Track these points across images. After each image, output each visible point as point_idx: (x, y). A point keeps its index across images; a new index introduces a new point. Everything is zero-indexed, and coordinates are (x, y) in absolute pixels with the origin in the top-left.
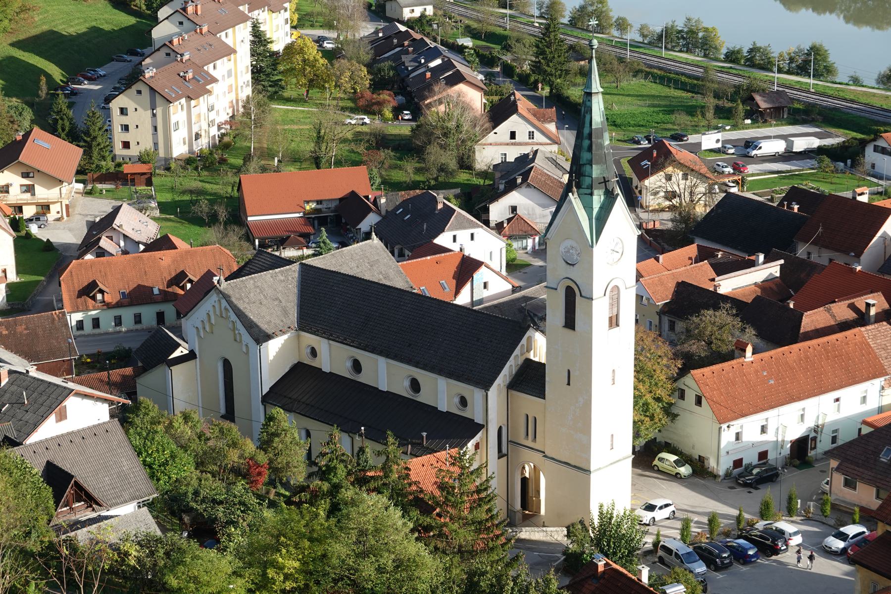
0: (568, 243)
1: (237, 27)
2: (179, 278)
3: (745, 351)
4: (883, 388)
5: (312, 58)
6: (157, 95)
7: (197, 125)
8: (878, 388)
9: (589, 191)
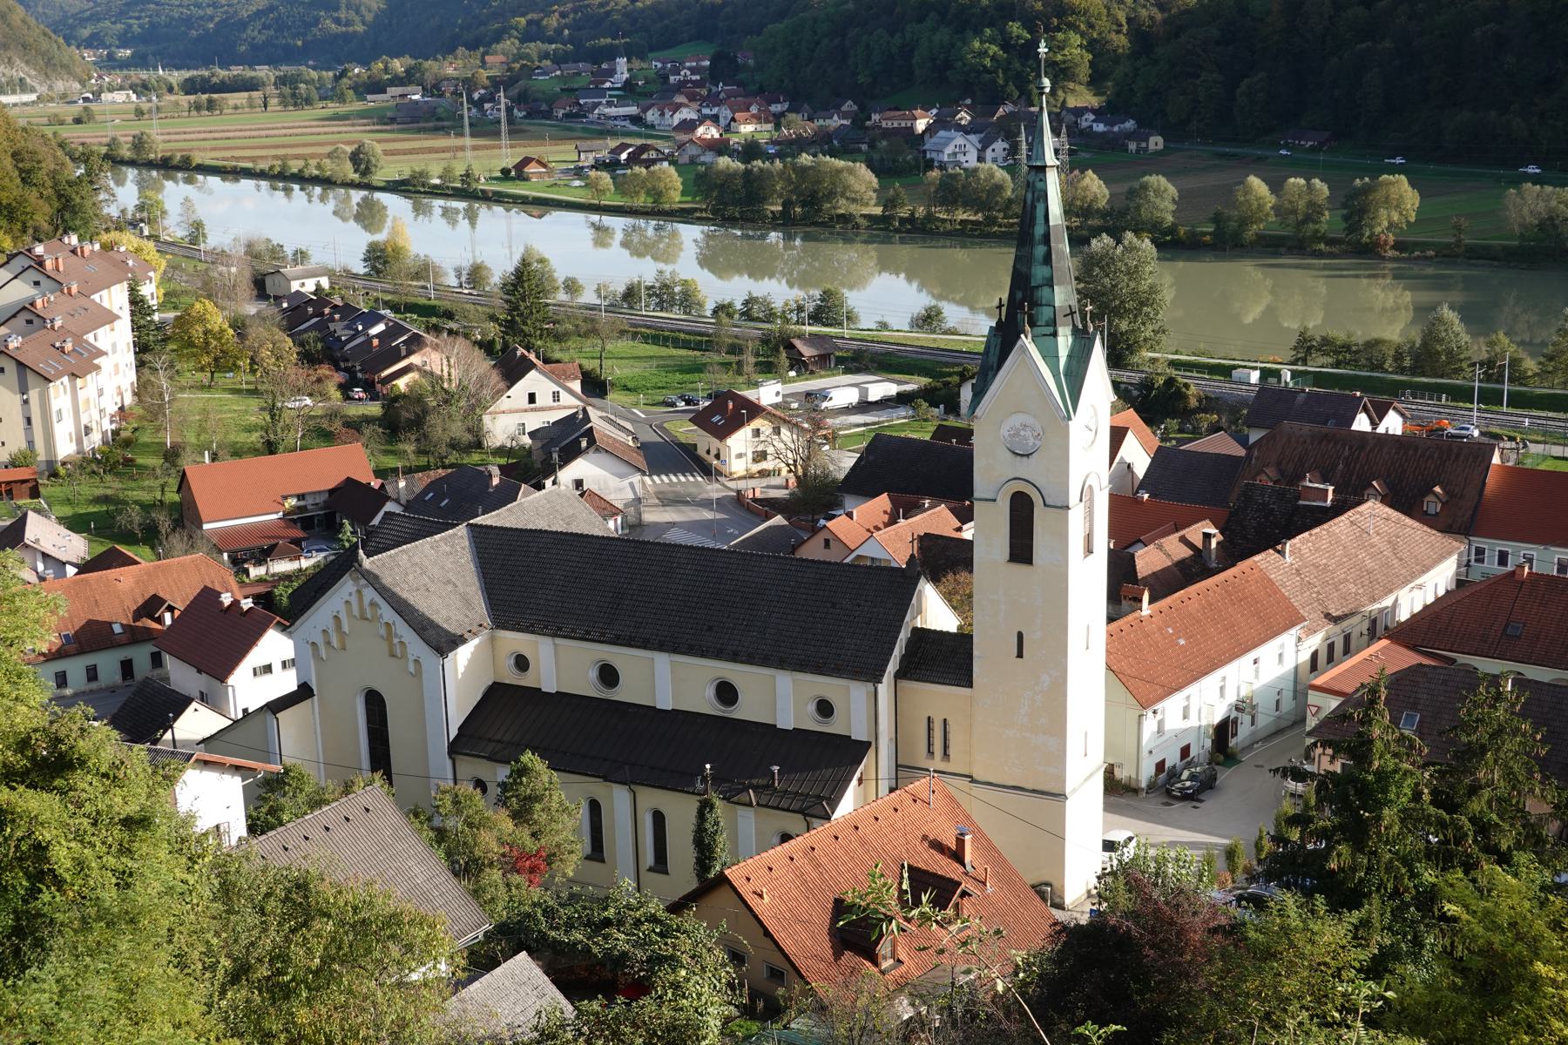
0: (1016, 420)
1: (113, 288)
2: (152, 606)
3: (1141, 601)
4: (1299, 639)
5: (217, 329)
6: (28, 371)
7: (86, 414)
8: (1294, 639)
9: (1051, 330)
